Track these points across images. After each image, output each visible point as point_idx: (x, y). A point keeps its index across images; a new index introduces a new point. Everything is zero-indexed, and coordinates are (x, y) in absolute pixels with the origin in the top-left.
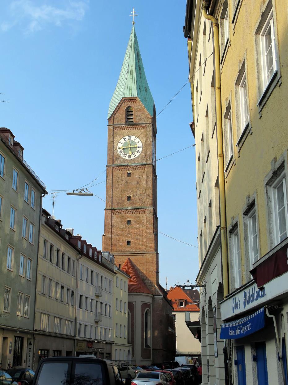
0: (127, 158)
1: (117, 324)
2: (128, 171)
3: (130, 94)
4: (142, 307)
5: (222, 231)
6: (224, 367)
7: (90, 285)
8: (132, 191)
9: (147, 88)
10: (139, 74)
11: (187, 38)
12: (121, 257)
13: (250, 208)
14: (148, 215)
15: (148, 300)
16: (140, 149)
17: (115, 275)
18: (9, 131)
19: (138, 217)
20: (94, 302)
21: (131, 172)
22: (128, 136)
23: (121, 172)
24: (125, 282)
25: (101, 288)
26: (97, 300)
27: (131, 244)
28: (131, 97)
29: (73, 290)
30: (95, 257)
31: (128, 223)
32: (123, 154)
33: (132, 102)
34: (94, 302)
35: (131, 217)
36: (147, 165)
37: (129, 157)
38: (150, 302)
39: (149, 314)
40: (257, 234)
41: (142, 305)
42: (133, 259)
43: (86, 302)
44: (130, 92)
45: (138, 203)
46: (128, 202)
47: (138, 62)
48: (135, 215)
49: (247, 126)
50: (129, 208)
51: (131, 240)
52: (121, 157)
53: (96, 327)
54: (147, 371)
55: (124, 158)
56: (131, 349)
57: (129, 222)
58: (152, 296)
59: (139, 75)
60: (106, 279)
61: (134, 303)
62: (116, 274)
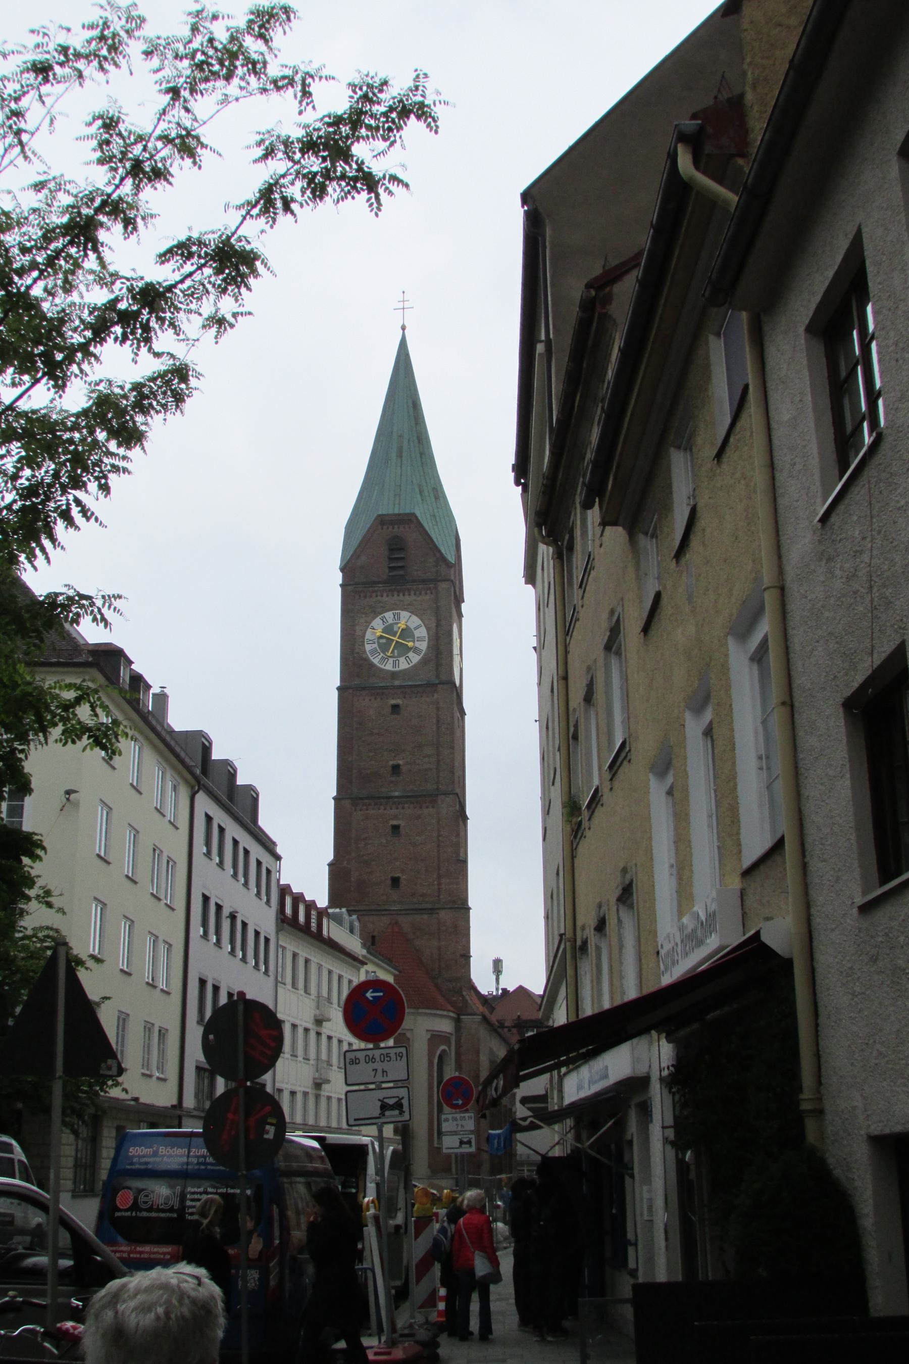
0: (389, 667)
2: (393, 702)
3: (397, 506)
5: (568, 944)
6: (70, 1246)
10: (418, 455)
11: (520, 487)
13: (601, 926)
15: (445, 1026)
16: (423, 646)
19: (418, 817)
25: (329, 1000)
26: (318, 1029)
27: (402, 885)
28: (399, 515)
30: (314, 925)
31: (393, 833)
33: (401, 594)
34: (312, 1035)
36: (440, 686)
41: (429, 1039)
42: (405, 922)
44: (397, 502)
46: (393, 779)
47: (416, 424)
49: (623, 745)
50: (397, 794)
53: (317, 1097)
55: (382, 667)
57: (396, 828)
60: (340, 977)
62: (363, 963)
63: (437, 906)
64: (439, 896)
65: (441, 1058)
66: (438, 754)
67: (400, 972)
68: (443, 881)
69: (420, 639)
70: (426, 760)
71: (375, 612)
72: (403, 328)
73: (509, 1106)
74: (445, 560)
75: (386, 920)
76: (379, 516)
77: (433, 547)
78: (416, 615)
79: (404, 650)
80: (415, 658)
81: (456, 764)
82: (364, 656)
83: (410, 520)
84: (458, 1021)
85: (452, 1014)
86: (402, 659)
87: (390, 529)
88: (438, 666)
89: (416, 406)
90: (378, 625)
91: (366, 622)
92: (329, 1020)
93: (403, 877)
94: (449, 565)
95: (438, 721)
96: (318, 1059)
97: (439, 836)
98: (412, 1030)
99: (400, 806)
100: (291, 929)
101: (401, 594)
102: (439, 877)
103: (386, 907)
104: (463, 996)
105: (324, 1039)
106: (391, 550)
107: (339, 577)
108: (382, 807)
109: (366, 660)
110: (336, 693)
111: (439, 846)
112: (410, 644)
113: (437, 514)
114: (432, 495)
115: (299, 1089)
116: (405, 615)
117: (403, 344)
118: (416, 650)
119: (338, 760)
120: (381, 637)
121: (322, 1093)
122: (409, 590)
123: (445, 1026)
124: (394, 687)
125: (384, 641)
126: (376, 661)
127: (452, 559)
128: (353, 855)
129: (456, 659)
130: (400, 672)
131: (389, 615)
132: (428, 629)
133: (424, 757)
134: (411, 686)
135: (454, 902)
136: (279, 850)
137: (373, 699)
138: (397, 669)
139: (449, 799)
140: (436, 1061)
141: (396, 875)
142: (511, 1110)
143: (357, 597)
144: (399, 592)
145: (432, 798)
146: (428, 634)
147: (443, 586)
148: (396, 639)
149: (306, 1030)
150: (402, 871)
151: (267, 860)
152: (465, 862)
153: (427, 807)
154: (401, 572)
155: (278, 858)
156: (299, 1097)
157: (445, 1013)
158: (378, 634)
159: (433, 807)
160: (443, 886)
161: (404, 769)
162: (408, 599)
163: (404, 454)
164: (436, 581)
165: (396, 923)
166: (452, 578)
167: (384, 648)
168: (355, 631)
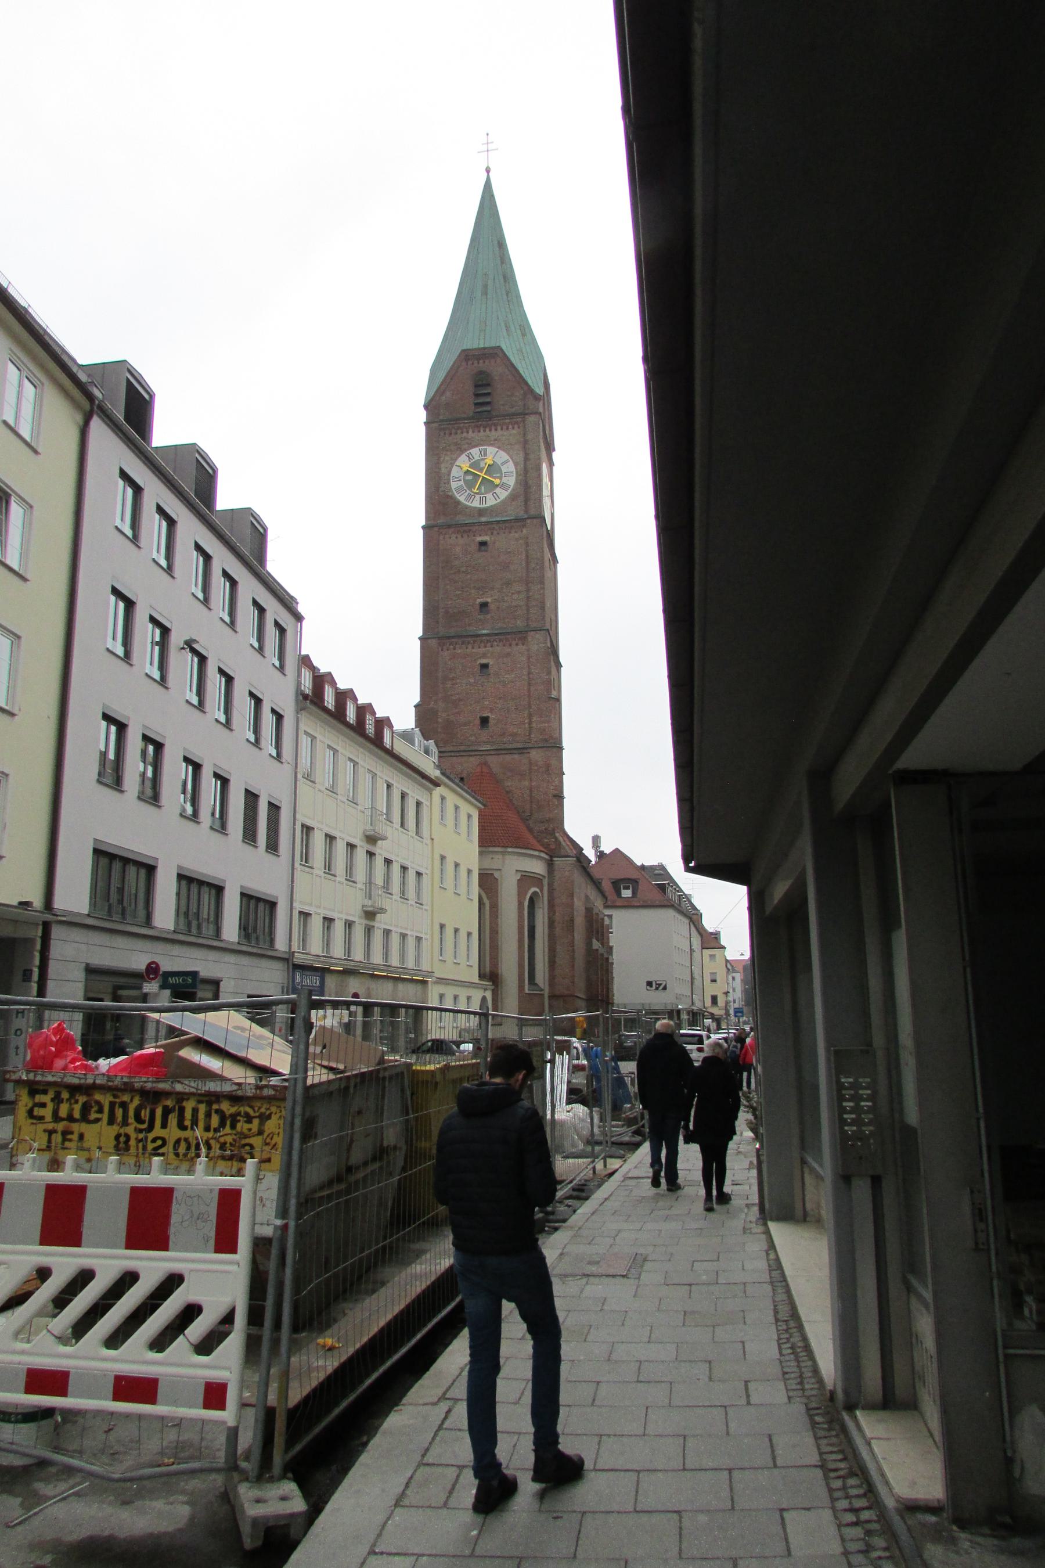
0: (476, 504)
1: (442, 926)
2: (480, 539)
4: (519, 887)
7: (413, 837)
8: (492, 589)
9: (526, 327)
10: (504, 293)
12: (465, 758)
14: (534, 648)
15: (537, 867)
16: (511, 481)
18: (125, 361)
19: (508, 655)
20: (360, 855)
22: (477, 449)
23: (461, 541)
24: (469, 816)
26: (372, 849)
28: (484, 348)
29: (404, 862)
32: (466, 494)
33: (487, 430)
34: (360, 855)
35: (490, 653)
36: (529, 521)
42: (495, 762)
43: (403, 883)
45: (507, 620)
46: (481, 617)
47: (502, 263)
48: (498, 649)
50: (485, 632)
51: (489, 714)
53: (369, 931)
55: (469, 504)
56: (489, 995)
57: (484, 666)
58: (545, 859)
59: (505, 297)
61: (496, 875)
63: (527, 745)
64: (530, 735)
65: (532, 901)
66: (528, 590)
67: (484, 805)
68: (534, 719)
69: (507, 475)
70: (515, 596)
71: (460, 449)
72: (488, 171)
73: (606, 956)
74: (531, 391)
75: (474, 761)
76: (464, 351)
77: (521, 381)
78: (503, 450)
79: (491, 486)
80: (503, 494)
81: (548, 604)
82: (450, 494)
83: (495, 354)
84: (550, 865)
85: (543, 855)
86: (489, 496)
87: (476, 364)
88: (526, 501)
89: (502, 245)
90: (463, 463)
91: (452, 459)
92: (384, 838)
93: (492, 716)
94: (537, 398)
95: (527, 556)
96: (370, 883)
97: (529, 673)
98: (500, 870)
99: (489, 644)
100: (314, 708)
101: (487, 430)
102: (530, 716)
103: (476, 748)
104: (556, 838)
105: (379, 862)
106: (476, 386)
107: (423, 416)
108: (470, 646)
109: (452, 497)
110: (421, 532)
111: (529, 684)
112: (497, 481)
113: (524, 350)
114: (519, 332)
115: (340, 919)
116: (491, 450)
117: (488, 188)
118: (503, 486)
119: (424, 600)
120: (467, 472)
121: (376, 924)
122: (495, 425)
123: (537, 867)
124: (480, 524)
125: (470, 478)
126: (462, 499)
127: (540, 390)
128: (440, 695)
129: (546, 501)
130: (489, 507)
131: (475, 452)
132: (516, 464)
133: (513, 594)
134: (498, 522)
135: (546, 740)
136: (301, 609)
137: (459, 536)
138: (484, 506)
139: (539, 636)
140: (526, 903)
142: (607, 959)
143: (442, 434)
144: (485, 427)
145: (521, 635)
146: (516, 469)
147: (532, 419)
148: (482, 475)
149: (351, 846)
150: (491, 710)
151: (286, 620)
152: (558, 700)
153: (517, 645)
154: (488, 408)
155: (299, 618)
156: (339, 928)
157: (536, 853)
158: (465, 469)
159: (523, 644)
160: (534, 725)
161: (492, 607)
162: (494, 434)
163: (489, 291)
164: (524, 415)
165: (486, 763)
166: (541, 410)
167: (470, 485)
168: (440, 469)
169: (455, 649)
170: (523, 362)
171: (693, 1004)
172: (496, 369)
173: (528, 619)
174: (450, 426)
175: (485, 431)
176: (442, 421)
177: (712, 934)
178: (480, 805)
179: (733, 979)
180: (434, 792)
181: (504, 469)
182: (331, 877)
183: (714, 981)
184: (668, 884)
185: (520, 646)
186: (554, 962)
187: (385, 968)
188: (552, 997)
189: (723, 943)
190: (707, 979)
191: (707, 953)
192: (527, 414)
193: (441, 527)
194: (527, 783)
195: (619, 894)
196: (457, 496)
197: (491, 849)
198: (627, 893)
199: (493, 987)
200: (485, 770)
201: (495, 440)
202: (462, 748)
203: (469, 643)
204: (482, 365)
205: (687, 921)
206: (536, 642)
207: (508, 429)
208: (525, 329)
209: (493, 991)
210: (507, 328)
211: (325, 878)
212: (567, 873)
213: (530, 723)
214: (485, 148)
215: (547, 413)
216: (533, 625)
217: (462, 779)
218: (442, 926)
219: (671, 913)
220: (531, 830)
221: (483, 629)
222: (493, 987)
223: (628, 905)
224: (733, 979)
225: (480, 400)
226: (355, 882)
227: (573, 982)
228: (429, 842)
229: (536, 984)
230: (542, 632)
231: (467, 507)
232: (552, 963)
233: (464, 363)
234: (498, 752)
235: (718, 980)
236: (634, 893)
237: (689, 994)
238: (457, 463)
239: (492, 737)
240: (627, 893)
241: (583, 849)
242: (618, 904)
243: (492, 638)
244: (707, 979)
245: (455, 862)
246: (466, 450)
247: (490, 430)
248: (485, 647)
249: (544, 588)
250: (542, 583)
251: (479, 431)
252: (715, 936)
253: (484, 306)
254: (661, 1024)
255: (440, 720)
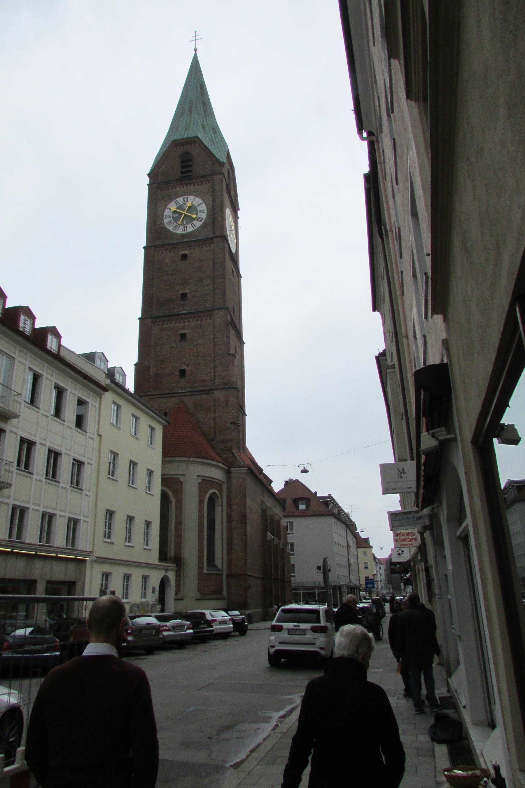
0: (180, 231)
2: (182, 253)
15: (217, 474)
16: (204, 216)
17: (102, 392)
21: (186, 252)
32: (174, 226)
33: (189, 186)
36: (215, 239)
37: (183, 230)
38: (222, 480)
39: (218, 503)
40: (468, 521)
42: (189, 401)
46: (182, 302)
48: (193, 323)
51: (186, 368)
52: (164, 224)
54: (459, 664)
55: (175, 232)
57: (183, 336)
61: (182, 479)
63: (213, 387)
68: (217, 369)
69: (201, 212)
70: (206, 288)
71: (171, 199)
72: (196, 50)
74: (218, 161)
78: (197, 197)
80: (198, 224)
82: (163, 226)
83: (194, 141)
84: (228, 473)
90: (173, 206)
93: (188, 369)
95: (214, 262)
97: (214, 338)
99: (186, 321)
101: (189, 186)
102: (215, 367)
104: (233, 454)
107: (147, 180)
108: (174, 322)
109: (165, 228)
111: (214, 346)
113: (214, 141)
114: (211, 131)
116: (191, 198)
120: (175, 212)
123: (217, 474)
126: (171, 228)
131: (180, 200)
132: (207, 205)
133: (204, 286)
135: (225, 384)
137: (168, 252)
138: (186, 232)
139: (222, 313)
141: (183, 368)
144: (187, 184)
145: (209, 313)
146: (207, 208)
147: (217, 177)
150: (187, 365)
153: (206, 319)
154: (190, 174)
159: (210, 319)
160: (217, 373)
161: (189, 296)
162: (193, 188)
165: (183, 402)
167: (176, 220)
169: (163, 325)
170: (213, 146)
171: (350, 582)
172: (194, 150)
173: (214, 302)
174: (164, 186)
175: (187, 187)
176: (159, 183)
177: (364, 539)
178: (164, 422)
179: (380, 568)
180: (103, 396)
181: (199, 209)
182: (28, 475)
183: (366, 568)
184: (330, 501)
185: (208, 320)
186: (231, 548)
187: (9, 544)
188: (229, 576)
189: (371, 544)
190: (362, 566)
191: (360, 551)
192: (215, 175)
193: (156, 247)
194: (212, 415)
195: (297, 507)
196: (168, 227)
197: (177, 459)
198: (302, 507)
199: (176, 568)
200: (181, 405)
201: (193, 192)
202: (167, 392)
203: (173, 320)
204: (187, 148)
205: (344, 526)
206: (219, 317)
207: (202, 184)
208: (216, 130)
209: (176, 571)
210: (203, 128)
211: (46, 483)
212: (241, 480)
213: (215, 372)
214: (194, 38)
215: (232, 183)
216: (217, 305)
217: (166, 414)
218: (110, 514)
219: (332, 520)
220: (214, 448)
221: (183, 310)
222: (176, 568)
223: (303, 515)
224: (380, 568)
225: (183, 170)
226: (82, 490)
227: (246, 564)
228: (96, 437)
229: (216, 566)
230: (223, 310)
231: (174, 234)
232: (230, 549)
233: (175, 148)
234: (192, 393)
235: (369, 568)
236: (307, 507)
237: (347, 574)
238: (168, 207)
239: (187, 383)
240: (302, 507)
241: (263, 470)
242: (297, 514)
243: (188, 316)
244: (362, 566)
245: (148, 470)
246: (174, 199)
247: (191, 186)
248: (184, 322)
249: (224, 282)
250: (224, 278)
251: (183, 187)
252: (367, 540)
253: (189, 117)
254: (348, 597)
255: (151, 373)
